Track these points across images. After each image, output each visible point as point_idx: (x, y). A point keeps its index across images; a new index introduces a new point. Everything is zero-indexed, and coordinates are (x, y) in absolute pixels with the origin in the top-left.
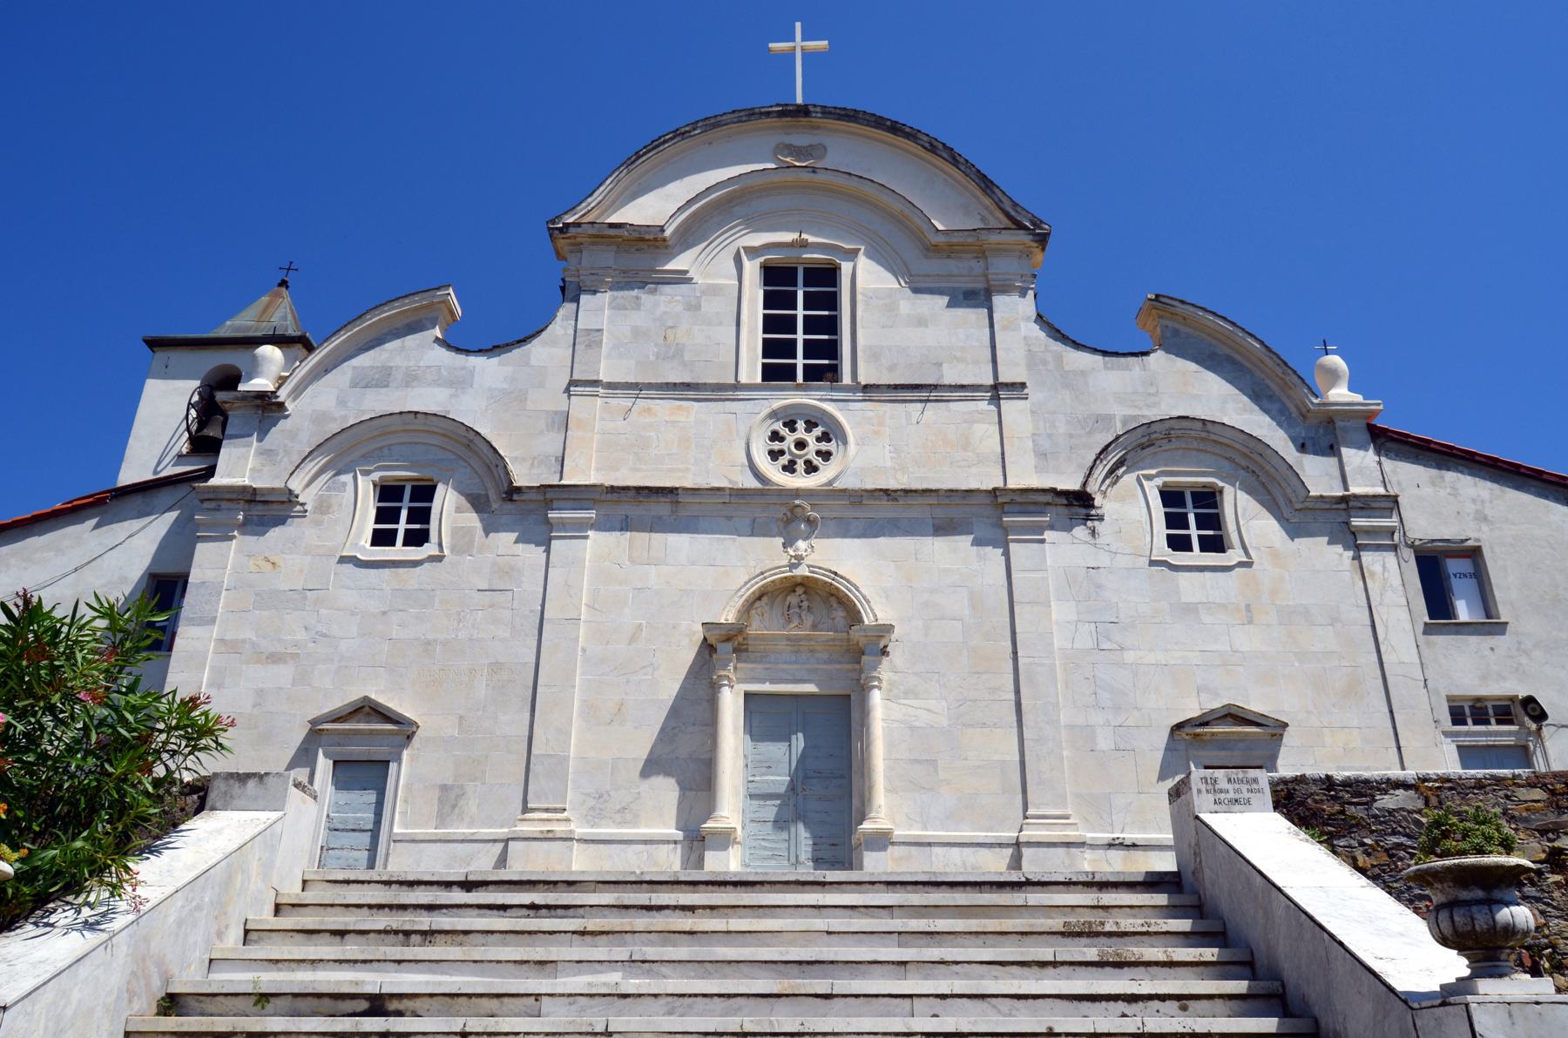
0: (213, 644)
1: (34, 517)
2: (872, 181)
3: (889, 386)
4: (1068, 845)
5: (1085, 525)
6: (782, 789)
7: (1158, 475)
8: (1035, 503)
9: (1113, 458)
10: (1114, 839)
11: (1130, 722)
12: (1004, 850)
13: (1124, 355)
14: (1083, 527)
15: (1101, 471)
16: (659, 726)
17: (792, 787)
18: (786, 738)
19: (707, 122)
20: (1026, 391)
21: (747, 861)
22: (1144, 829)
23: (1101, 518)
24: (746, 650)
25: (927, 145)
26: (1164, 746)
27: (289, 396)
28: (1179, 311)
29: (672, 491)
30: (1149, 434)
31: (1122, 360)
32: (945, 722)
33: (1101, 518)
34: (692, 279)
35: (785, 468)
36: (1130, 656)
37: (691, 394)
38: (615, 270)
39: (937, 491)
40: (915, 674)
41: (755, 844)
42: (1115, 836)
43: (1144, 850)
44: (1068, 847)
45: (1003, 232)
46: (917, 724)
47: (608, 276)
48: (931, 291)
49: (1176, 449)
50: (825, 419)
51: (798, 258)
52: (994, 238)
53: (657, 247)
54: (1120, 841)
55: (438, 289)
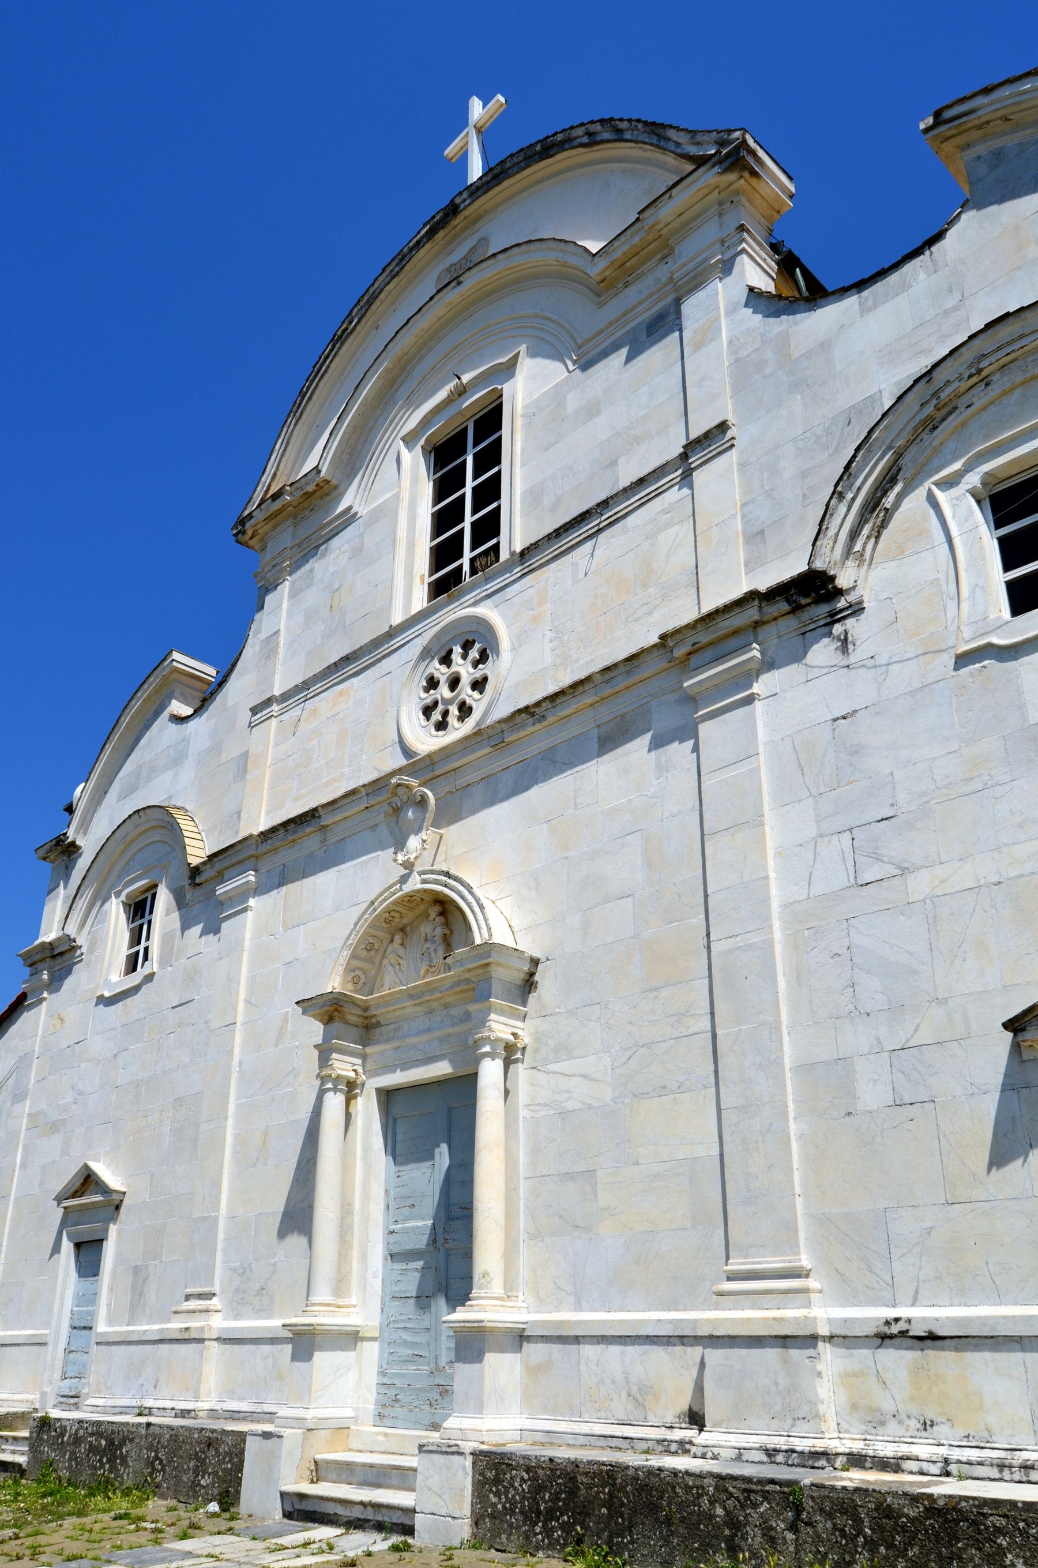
0: (25, 1120)
1: (10, 1006)
2: (542, 240)
3: (549, 537)
4: (785, 1341)
5: (830, 634)
6: (422, 1242)
7: (967, 469)
8: (735, 633)
9: (866, 482)
10: (887, 1323)
11: (924, 1036)
12: (689, 1349)
13: (896, 266)
14: (826, 641)
15: (844, 517)
16: (295, 1160)
17: (433, 1240)
18: (427, 1155)
19: (361, 303)
20: (729, 434)
21: (385, 1366)
22: (962, 1295)
23: (857, 609)
24: (378, 1025)
25: (585, 140)
26: (1000, 1079)
27: (77, 832)
28: (984, 115)
29: (311, 815)
30: (935, 394)
31: (893, 278)
32: (607, 1094)
33: (857, 609)
34: (356, 513)
35: (461, 719)
36: (920, 885)
37: (351, 668)
38: (292, 548)
39: (588, 679)
40: (571, 1013)
41: (394, 1337)
42: (891, 1313)
43: (957, 1349)
44: (785, 1347)
45: (674, 192)
46: (570, 1105)
47: (284, 562)
48: (605, 354)
49: (1005, 393)
50: (445, 639)
51: (460, 413)
52: (666, 212)
53: (328, 494)
54: (902, 1326)
55: (164, 660)
